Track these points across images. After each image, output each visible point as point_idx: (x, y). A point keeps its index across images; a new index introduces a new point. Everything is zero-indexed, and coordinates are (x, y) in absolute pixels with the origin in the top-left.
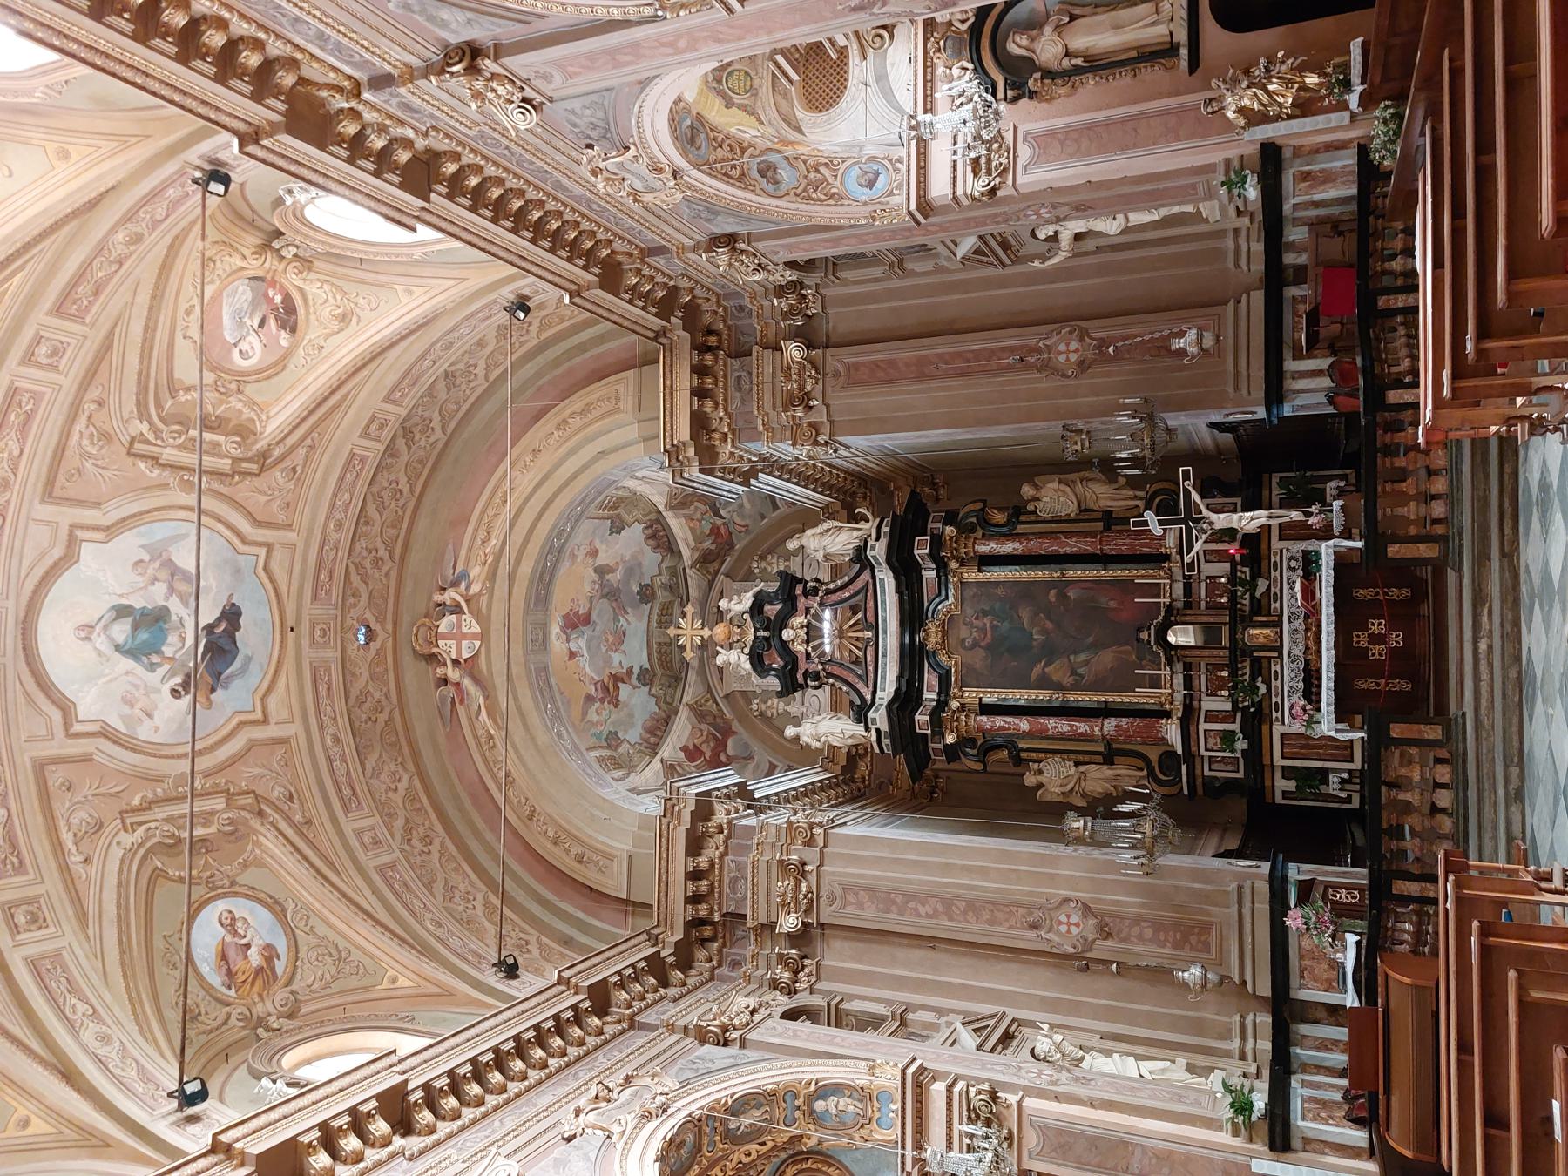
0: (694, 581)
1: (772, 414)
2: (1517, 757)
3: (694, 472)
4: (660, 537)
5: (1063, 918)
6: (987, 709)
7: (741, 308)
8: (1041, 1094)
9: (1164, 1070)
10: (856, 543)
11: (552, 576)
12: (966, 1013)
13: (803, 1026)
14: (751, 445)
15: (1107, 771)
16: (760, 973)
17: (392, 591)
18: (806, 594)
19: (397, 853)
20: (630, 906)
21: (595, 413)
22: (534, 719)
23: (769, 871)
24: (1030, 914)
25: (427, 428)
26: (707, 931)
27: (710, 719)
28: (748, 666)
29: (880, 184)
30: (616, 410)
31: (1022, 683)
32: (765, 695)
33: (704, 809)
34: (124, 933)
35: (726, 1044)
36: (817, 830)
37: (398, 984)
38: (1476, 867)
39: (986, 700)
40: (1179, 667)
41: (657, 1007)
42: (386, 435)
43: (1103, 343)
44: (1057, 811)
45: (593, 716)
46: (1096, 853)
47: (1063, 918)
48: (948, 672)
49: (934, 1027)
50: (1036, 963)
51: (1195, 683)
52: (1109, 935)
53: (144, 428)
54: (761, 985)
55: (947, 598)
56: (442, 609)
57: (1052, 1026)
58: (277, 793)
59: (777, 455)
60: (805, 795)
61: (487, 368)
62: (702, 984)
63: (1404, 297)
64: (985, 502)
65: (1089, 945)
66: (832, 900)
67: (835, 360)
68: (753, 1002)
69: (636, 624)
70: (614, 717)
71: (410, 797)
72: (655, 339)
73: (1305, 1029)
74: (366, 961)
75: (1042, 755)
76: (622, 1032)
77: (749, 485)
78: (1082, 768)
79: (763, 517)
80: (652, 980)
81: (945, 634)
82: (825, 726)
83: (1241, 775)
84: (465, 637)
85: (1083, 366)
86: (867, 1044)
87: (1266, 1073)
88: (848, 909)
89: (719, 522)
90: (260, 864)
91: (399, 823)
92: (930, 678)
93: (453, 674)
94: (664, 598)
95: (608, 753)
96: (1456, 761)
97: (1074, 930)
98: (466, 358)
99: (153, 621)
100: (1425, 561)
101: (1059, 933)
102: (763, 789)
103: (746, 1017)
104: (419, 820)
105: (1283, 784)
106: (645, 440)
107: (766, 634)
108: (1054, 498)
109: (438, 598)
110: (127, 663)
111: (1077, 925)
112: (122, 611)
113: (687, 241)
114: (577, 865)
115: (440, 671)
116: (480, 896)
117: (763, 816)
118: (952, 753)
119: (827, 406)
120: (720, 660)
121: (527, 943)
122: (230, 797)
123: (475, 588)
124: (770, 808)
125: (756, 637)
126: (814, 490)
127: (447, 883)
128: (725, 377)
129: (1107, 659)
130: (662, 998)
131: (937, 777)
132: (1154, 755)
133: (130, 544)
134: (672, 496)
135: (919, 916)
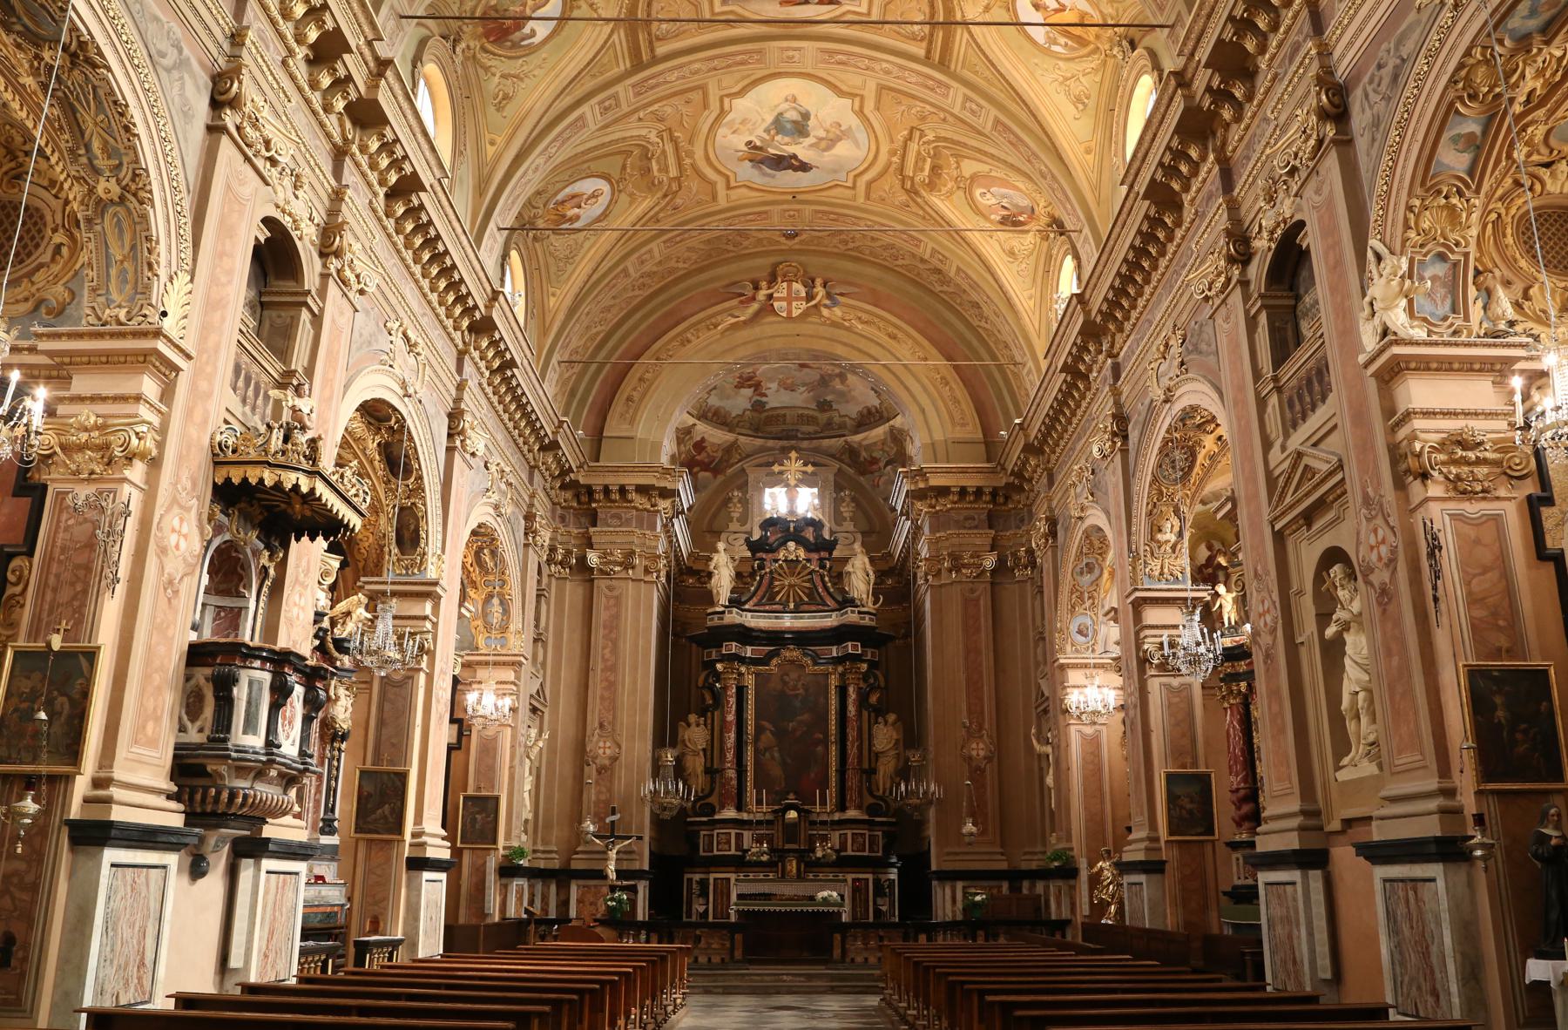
1: (947, 544)
2: (728, 991)
4: (869, 418)
6: (741, 691)
8: (514, 737)
15: (700, 769)
18: (821, 559)
25: (943, 283)
26: (584, 499)
29: (1080, 639)
34: (596, 148)
40: (769, 817)
46: (648, 766)
52: (599, 772)
53: (931, 137)
56: (810, 284)
58: (678, 201)
66: (610, 588)
67: (983, 589)
71: (671, 271)
73: (553, 888)
81: (792, 662)
84: (790, 304)
89: (882, 464)
90: (631, 204)
93: (762, 295)
99: (800, 129)
105: (697, 877)
108: (885, 736)
109: (819, 282)
110: (770, 119)
112: (806, 116)
113: (1054, 503)
115: (764, 284)
122: (678, 179)
123: (825, 312)
130: (482, 374)
132: (713, 800)
133: (852, 121)
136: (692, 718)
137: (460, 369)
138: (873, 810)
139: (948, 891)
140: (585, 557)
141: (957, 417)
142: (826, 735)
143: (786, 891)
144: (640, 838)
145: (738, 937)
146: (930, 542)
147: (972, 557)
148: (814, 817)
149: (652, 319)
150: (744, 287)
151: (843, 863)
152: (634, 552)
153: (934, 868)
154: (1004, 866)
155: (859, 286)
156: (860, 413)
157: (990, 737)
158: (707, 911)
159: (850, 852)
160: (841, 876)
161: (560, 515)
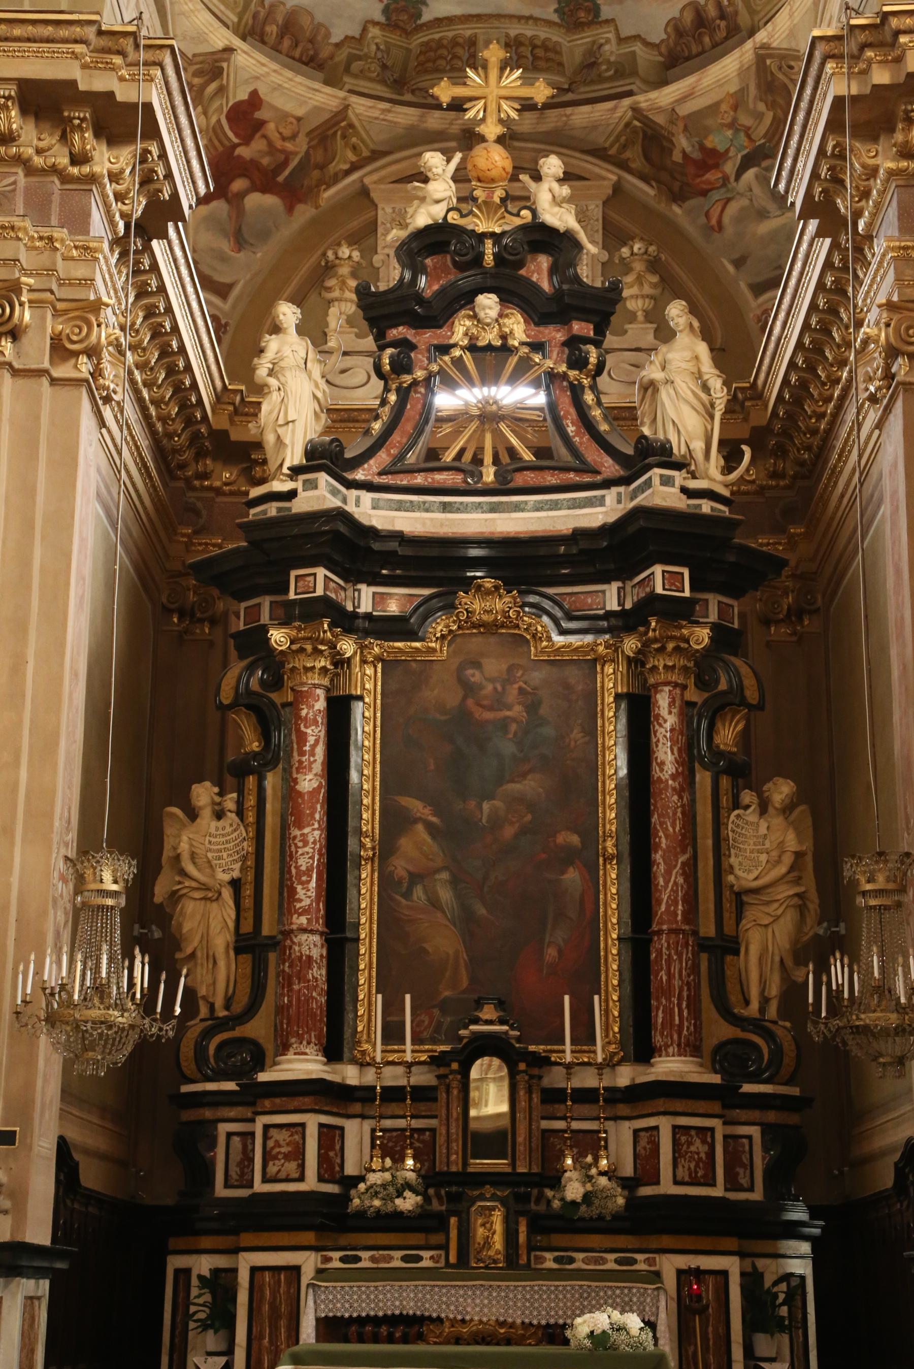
0: (601, 117)
3: (838, 85)
10: (678, 450)
14: (892, 214)
15: (222, 940)
18: (573, 343)
28: (422, 219)
31: (394, 778)
33: (121, 122)
36: (85, 366)
39: (358, 708)
40: (423, 1077)
46: (57, 919)
48: (412, 635)
51: (394, 1108)
55: (563, 632)
64: (760, 707)
75: (251, 817)
77: (805, 215)
78: (227, 894)
79: (739, 263)
81: (489, 628)
82: (298, 391)
83: (220, 1191)
89: (730, 168)
92: (396, 601)
102: (169, 255)
105: (204, 1265)
107: (489, 259)
108: (763, 844)
118: (254, 642)
120: (433, 160)
125: (482, 236)
126: (792, 364)
129: (443, 942)
131: (213, 622)
132: (258, 1028)
134: (786, 58)
136: (203, 794)
138: (732, 1059)
142: (590, 832)
148: (555, 1078)
151: (647, 1220)
152: (16, 287)
156: (675, 26)
159: (667, 1187)
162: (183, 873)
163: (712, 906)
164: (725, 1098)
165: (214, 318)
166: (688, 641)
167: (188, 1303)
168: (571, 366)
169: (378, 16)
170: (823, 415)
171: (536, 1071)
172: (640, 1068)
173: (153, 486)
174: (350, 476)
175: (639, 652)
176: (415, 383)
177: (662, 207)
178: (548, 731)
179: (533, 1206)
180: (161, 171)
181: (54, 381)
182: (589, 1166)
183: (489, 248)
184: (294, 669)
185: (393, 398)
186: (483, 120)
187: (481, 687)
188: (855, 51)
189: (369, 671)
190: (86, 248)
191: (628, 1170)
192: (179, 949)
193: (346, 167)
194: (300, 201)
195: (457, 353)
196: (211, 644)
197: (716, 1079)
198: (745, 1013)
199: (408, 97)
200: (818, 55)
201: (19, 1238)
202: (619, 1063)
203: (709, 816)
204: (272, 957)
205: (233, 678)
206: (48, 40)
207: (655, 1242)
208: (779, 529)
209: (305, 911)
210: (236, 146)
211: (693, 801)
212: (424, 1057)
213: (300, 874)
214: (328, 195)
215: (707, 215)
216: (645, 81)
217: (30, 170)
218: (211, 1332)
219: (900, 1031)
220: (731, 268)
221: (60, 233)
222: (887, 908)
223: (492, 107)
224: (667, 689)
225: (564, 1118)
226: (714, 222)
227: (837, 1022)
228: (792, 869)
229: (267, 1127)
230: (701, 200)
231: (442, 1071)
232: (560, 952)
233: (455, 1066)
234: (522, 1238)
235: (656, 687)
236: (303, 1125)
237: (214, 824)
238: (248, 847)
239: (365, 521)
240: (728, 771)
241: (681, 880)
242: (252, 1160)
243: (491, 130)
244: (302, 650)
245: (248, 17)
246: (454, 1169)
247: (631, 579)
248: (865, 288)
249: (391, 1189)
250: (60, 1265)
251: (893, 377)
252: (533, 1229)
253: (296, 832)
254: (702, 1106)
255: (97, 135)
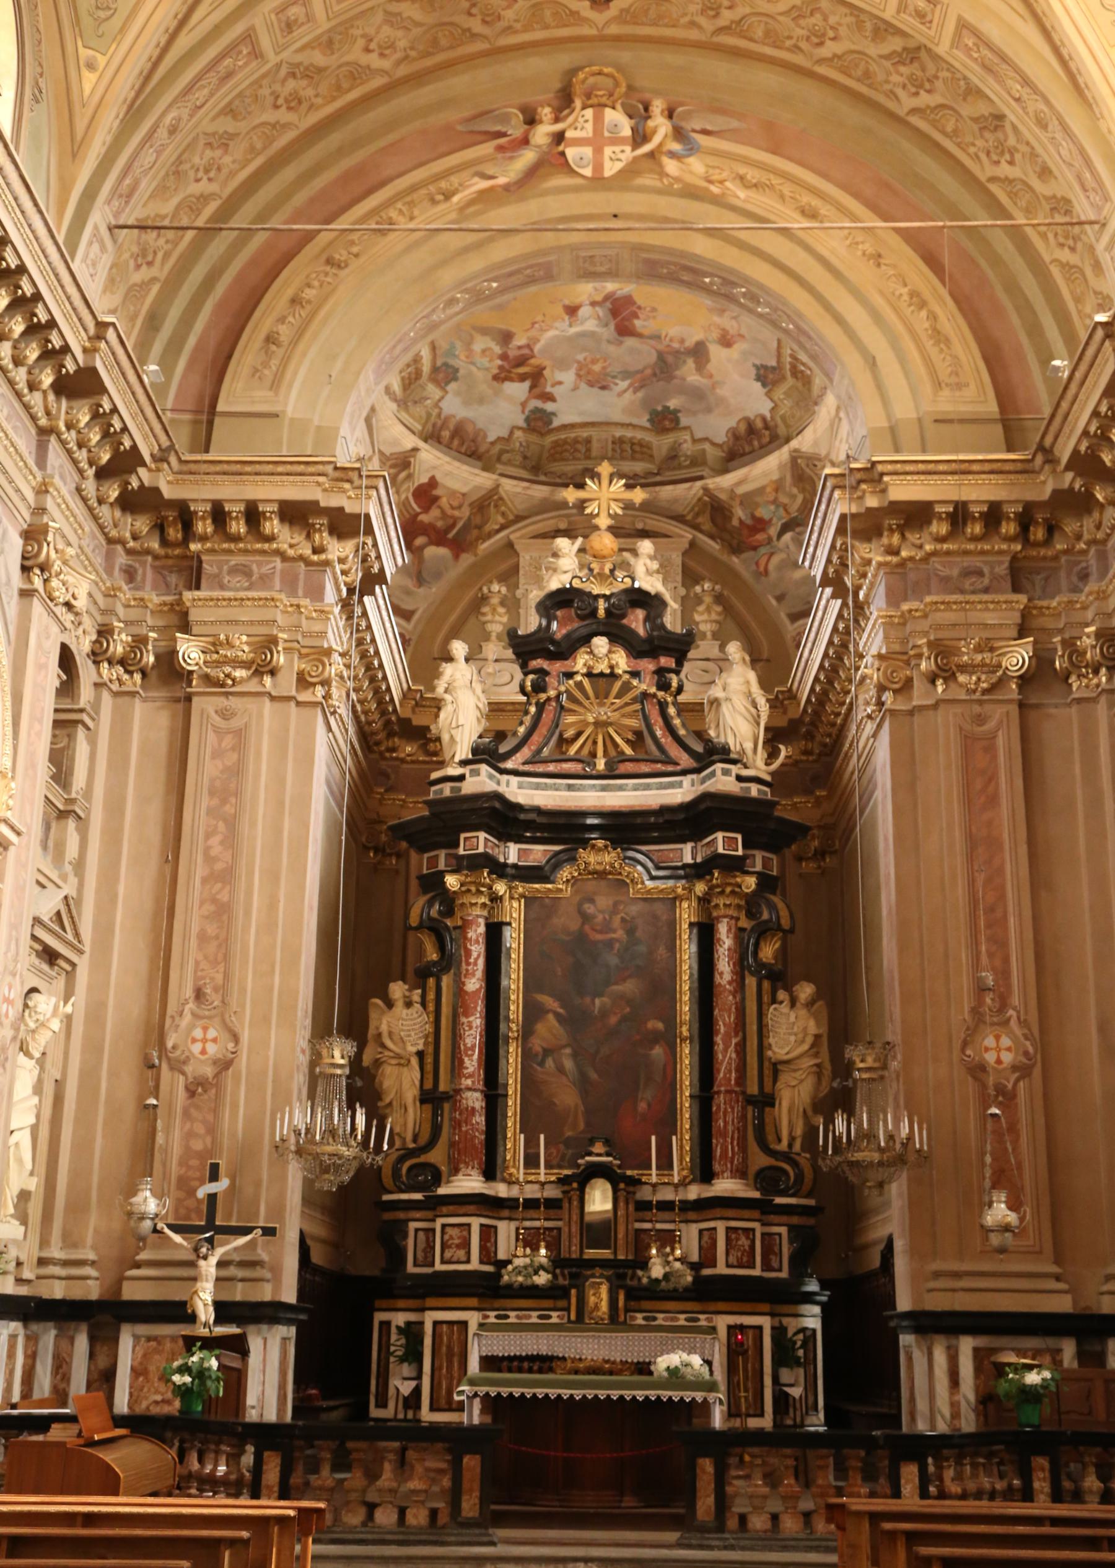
0: (681, 494)
1: (924, 625)
3: (841, 505)
4: (750, 441)
5: (212, 1033)
6: (494, 932)
7: (1084, 577)
9: (20, 1161)
11: (688, 284)
12: (79, 901)
13: (53, 676)
14: (881, 590)
15: (411, 1093)
16: (121, 611)
17: (669, 32)
18: (660, 672)
19: (273, 59)
20: (206, 415)
21: (933, 352)
22: (476, 263)
23: (261, 623)
24: (216, 989)
25: (917, 85)
26: (174, 533)
27: (477, 520)
28: (554, 585)
30: (938, 385)
31: (532, 983)
32: (512, 604)
33: (346, 525)
35: (25, 569)
36: (320, 691)
37: (85, 73)
38: (305, 1549)
39: (507, 932)
40: (552, 1192)
41: (68, 466)
42: (908, 22)
43: (1006, 1097)
44: (355, 1027)
45: (481, 343)
46: (300, 1081)
47: (212, 1033)
48: (546, 879)
49: (58, 857)
50: (149, 996)
51: (532, 1213)
52: (191, 1093)
54: (104, 612)
55: (653, 878)
56: (640, 113)
57: (69, 1018)
59: (862, 628)
60: (369, 668)
61: (1008, 181)
62: (101, 528)
63: (1047, 1490)
64: (792, 931)
65: (178, 1066)
67: (1001, 717)
68: (81, 603)
69: (618, 406)
70: (480, 375)
71: (358, 73)
72: (1041, 448)
73: (82, 1342)
74: (116, 22)
75: (431, 1007)
76: (34, 418)
78: (414, 1061)
79: (780, 598)
80: (105, 457)
81: (601, 875)
82: (467, 699)
83: (411, 1269)
84: (598, 151)
85: (978, 1070)
86: (33, 766)
87: (23, 1291)
88: (211, 737)
89: (773, 531)
91: (318, 58)
92: (539, 853)
93: (542, 134)
94: (654, 453)
95: (426, 368)
96: (434, 1530)
97: (196, 1048)
98: (1023, 148)
100: (691, 1505)
101: (192, 1027)
103: (61, 596)
104: (323, 89)
105: (400, 1319)
106: (893, 430)
107: (601, 612)
108: (792, 1029)
109: (658, 106)
111: (203, 1052)
114: (262, 336)
115: (546, 112)
116: (214, 187)
117: (337, 610)
118: (433, 883)
119: (935, 706)
120: (562, 543)
121: (150, 264)
123: (671, 166)
124: (350, 618)
125: (597, 597)
126: (816, 679)
127: (232, 136)
128: (983, 553)
129: (567, 1097)
130: (81, 472)
131: (399, 856)
132: (437, 1156)
135: (208, 836)
136: (397, 990)
137: (41, 461)
138: (768, 1180)
139: (940, 1357)
140: (174, 652)
141: (944, 370)
142: (670, 1018)
143: (588, 1350)
144: (269, 1232)
145: (471, 1463)
146: (888, 624)
147: (978, 649)
149: (319, 183)
150: (506, 119)
151: (707, 1291)
153: (904, 1303)
154: (1062, 1304)
155: (741, 116)
156: (734, 434)
157: (1023, 1023)
158: (417, 1391)
159: (721, 1269)
160: (703, 1320)
161: (123, 560)
162: (383, 1046)
163: (756, 1072)
164: (763, 1208)
165: (401, 635)
166: (740, 886)
167: (388, 1345)
168: (659, 688)
169: (521, 423)
170: (839, 714)
171: (631, 1189)
172: (705, 1187)
173: (359, 762)
174: (502, 765)
175: (706, 893)
176: (549, 699)
177: (725, 557)
178: (642, 949)
179: (629, 1282)
180: (373, 554)
181: (298, 704)
182: (668, 1255)
183: (602, 605)
184: (463, 904)
185: (533, 709)
186: (598, 515)
187: (594, 917)
188: (854, 483)
189: (515, 904)
190: (322, 611)
191: (695, 1257)
192: (381, 1099)
193: (497, 527)
194: (463, 551)
195: (578, 678)
196: (397, 872)
197: (757, 1195)
198: (779, 1148)
199: (542, 478)
200: (829, 484)
201: (277, 1299)
202: (690, 1183)
203: (755, 1008)
204: (447, 1106)
205: (418, 907)
206: (301, 474)
207: (712, 1306)
208: (808, 792)
209: (470, 1076)
210: (418, 514)
211: (743, 999)
212: (553, 1178)
213: (467, 1049)
214: (484, 547)
215: (757, 564)
216: (712, 469)
217: (284, 557)
218: (406, 1365)
219: (881, 1164)
220: (774, 602)
221: (305, 602)
222: (873, 1080)
223: (604, 506)
224: (726, 920)
225: (651, 1221)
226: (762, 569)
227: (838, 1159)
228: (812, 1046)
229: (444, 1226)
230: (751, 553)
231: (566, 1188)
232: (649, 1105)
233: (575, 1185)
234: (621, 1303)
235: (718, 918)
236: (469, 1225)
237: (405, 1011)
238: (429, 1028)
239: (512, 798)
240: (767, 977)
241: (734, 1056)
242: (433, 1248)
243: (603, 522)
244: (469, 891)
245: (429, 427)
246: (574, 1256)
247: (701, 840)
248: (865, 635)
249: (530, 1270)
250: (303, 1317)
251: (883, 704)
252: (628, 1298)
253: (464, 1020)
254: (746, 1213)
255: (331, 533)
